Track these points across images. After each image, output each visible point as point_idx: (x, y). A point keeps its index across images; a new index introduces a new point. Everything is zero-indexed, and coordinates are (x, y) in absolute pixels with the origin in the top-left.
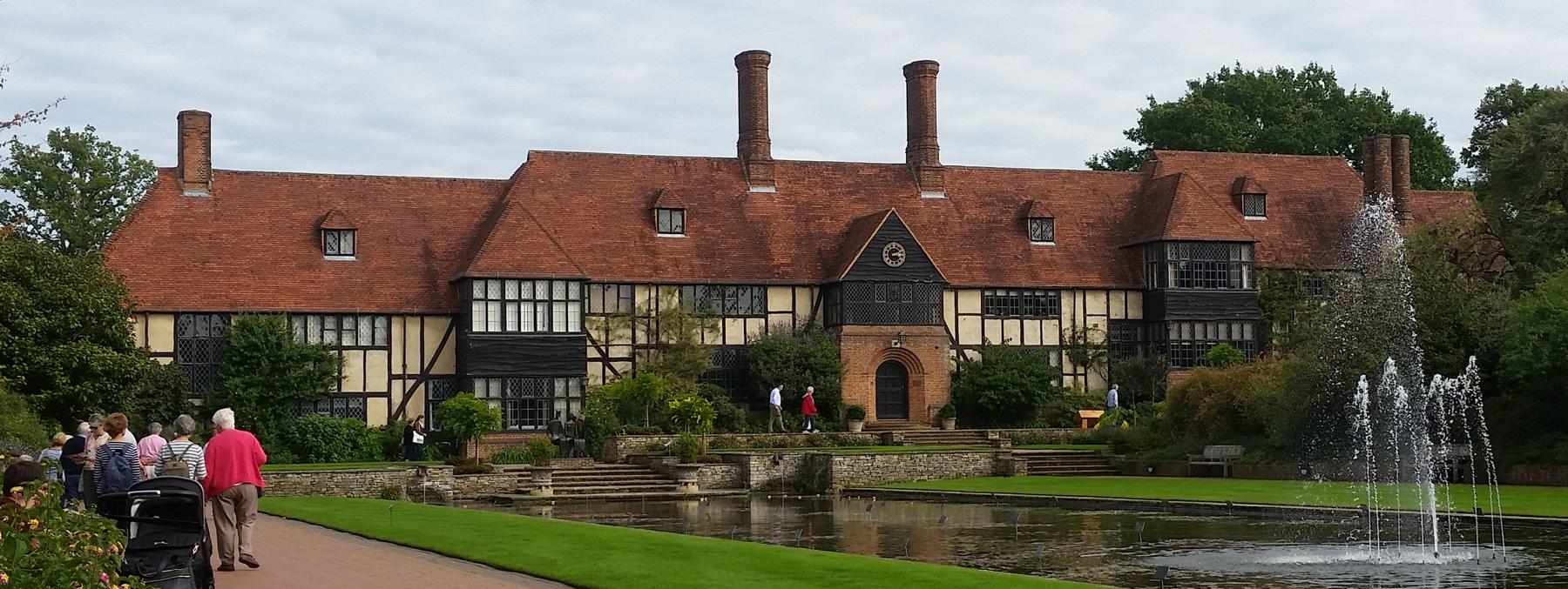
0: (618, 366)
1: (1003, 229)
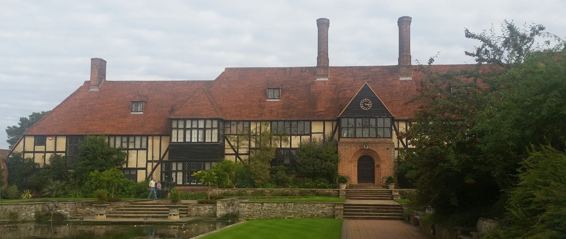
0: (242, 157)
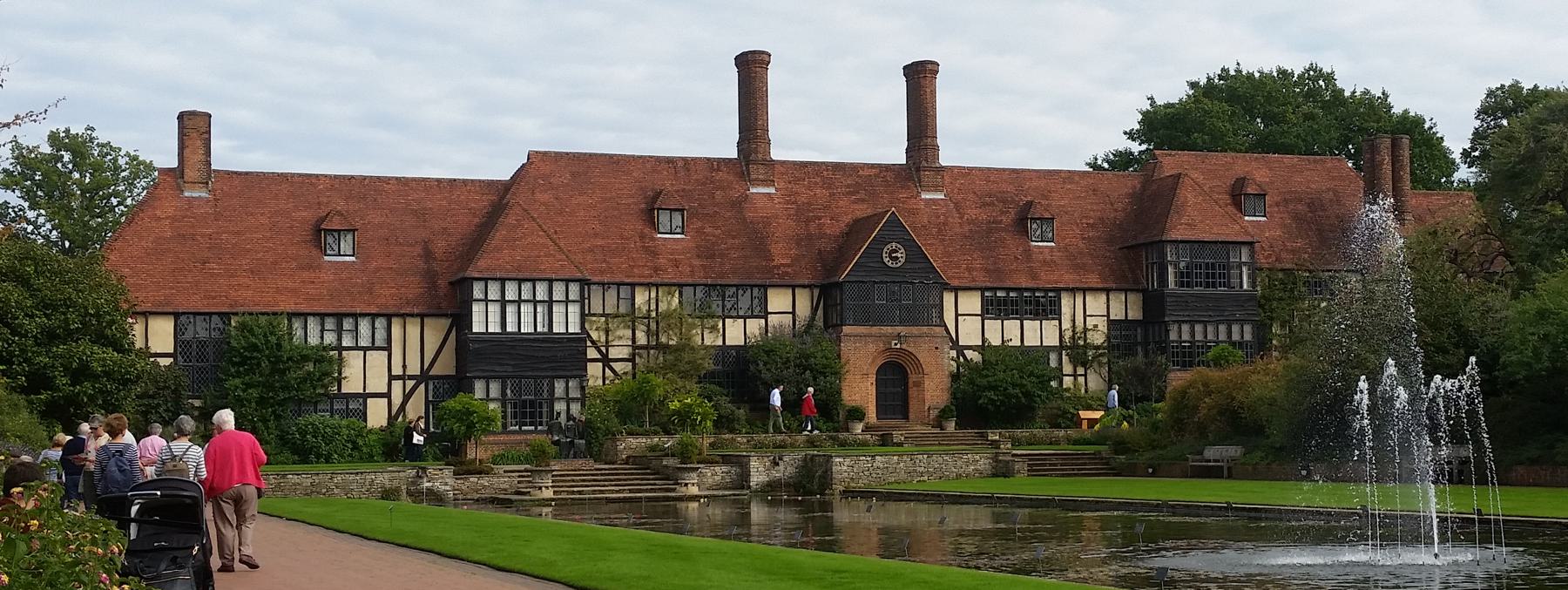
0: (618, 366)
1: (1003, 230)
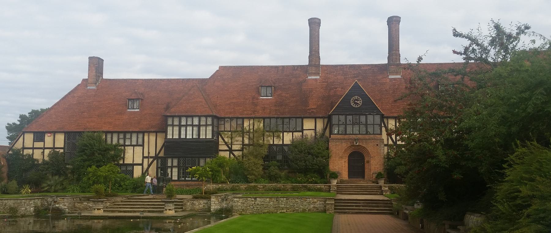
0: (236, 153)
